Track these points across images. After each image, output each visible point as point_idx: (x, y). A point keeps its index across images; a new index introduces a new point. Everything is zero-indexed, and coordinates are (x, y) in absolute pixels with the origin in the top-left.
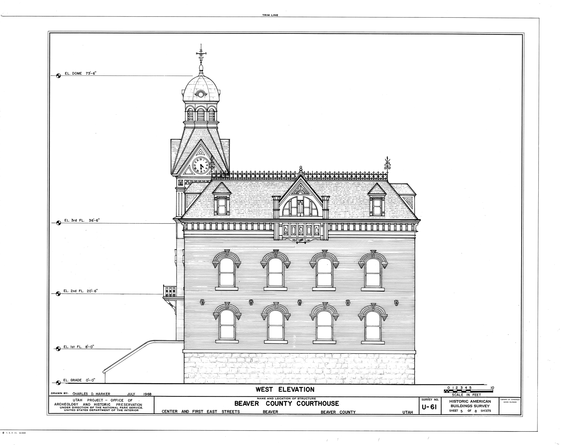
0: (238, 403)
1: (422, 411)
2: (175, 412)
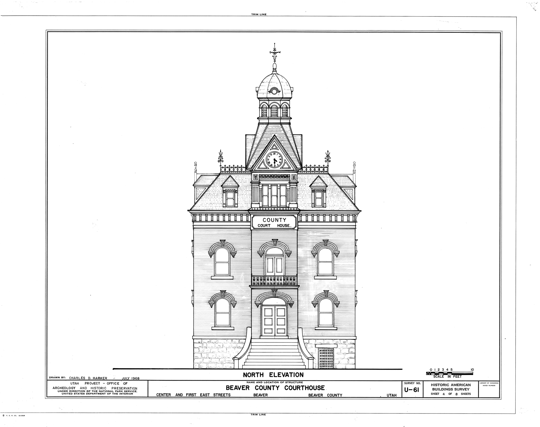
0: (229, 388)
1: (405, 394)
2: (168, 396)
